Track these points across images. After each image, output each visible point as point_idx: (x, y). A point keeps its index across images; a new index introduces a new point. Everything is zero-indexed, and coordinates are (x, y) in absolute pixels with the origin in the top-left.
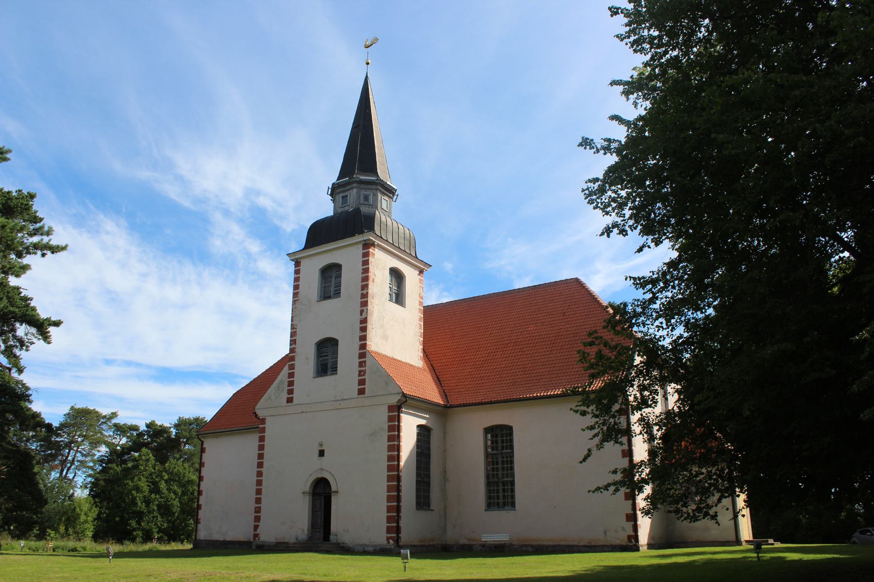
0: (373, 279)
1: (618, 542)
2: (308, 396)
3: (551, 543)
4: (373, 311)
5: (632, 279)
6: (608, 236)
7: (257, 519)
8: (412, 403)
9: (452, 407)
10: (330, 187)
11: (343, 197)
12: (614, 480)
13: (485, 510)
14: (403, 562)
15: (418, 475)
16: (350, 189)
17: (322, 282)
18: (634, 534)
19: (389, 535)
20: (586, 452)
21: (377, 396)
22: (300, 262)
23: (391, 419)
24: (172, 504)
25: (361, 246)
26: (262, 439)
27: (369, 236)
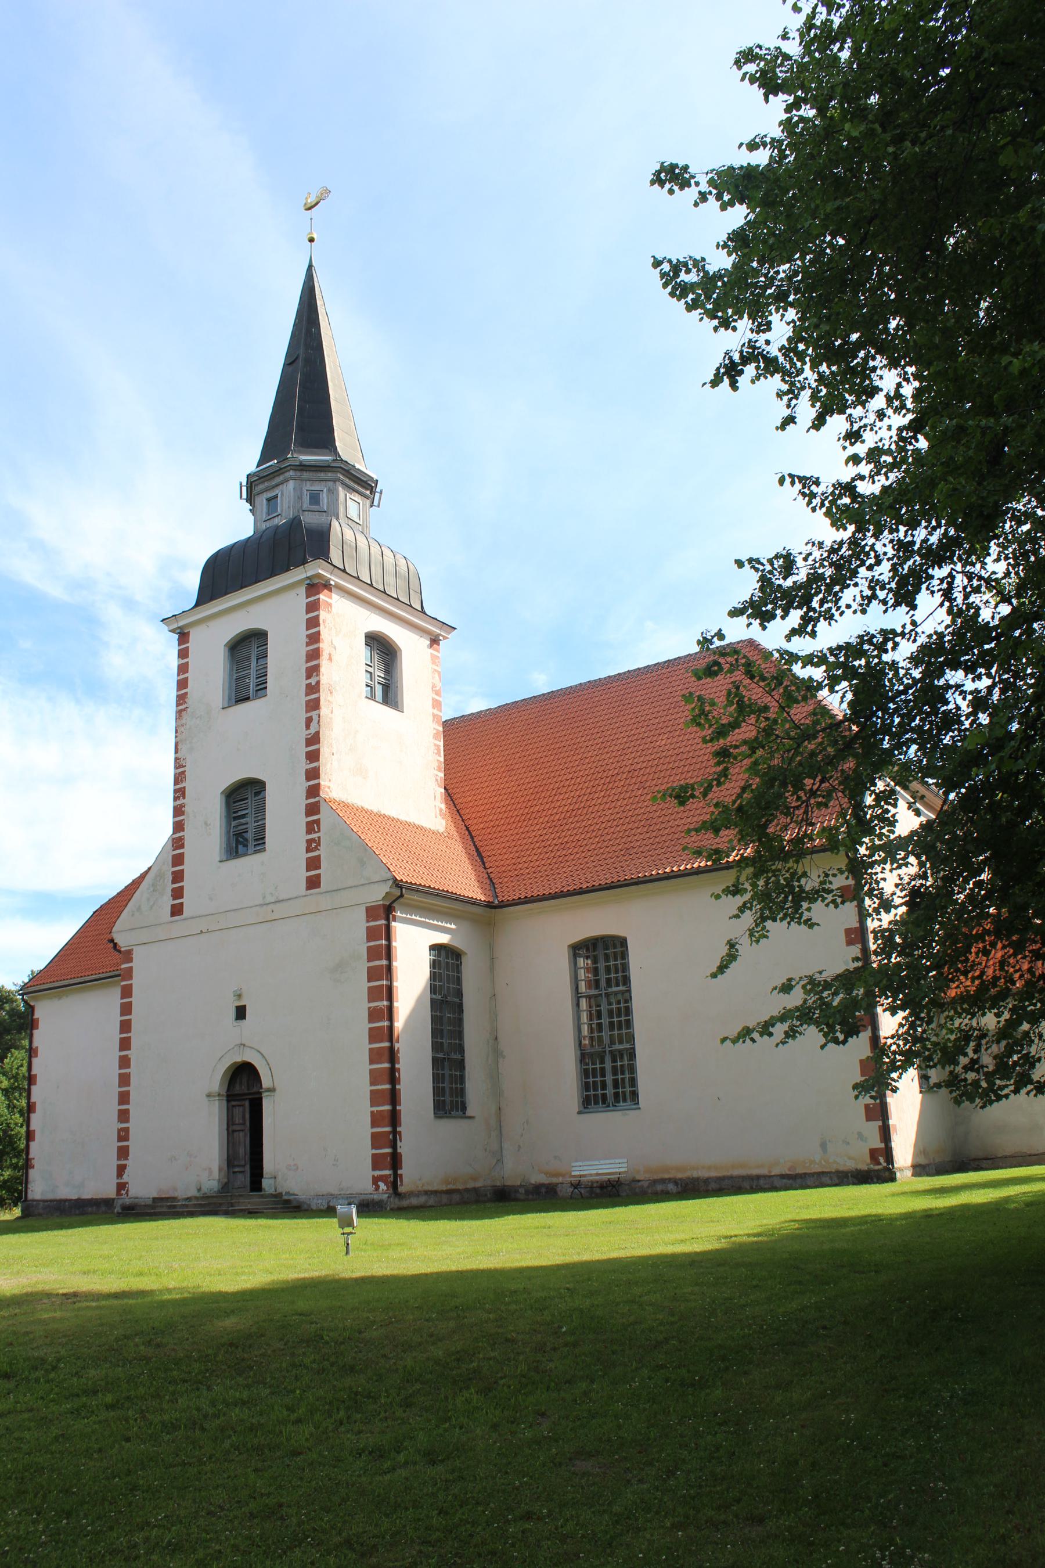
0: (330, 654)
1: (849, 1165)
2: (211, 899)
3: (713, 1174)
4: (331, 719)
5: (796, 480)
6: (734, 386)
7: (123, 1153)
8: (417, 901)
9: (502, 905)
10: (244, 483)
11: (269, 500)
12: (784, 1008)
13: (579, 1113)
14: (344, 1234)
15: (436, 1047)
16: (282, 483)
17: (231, 670)
18: (883, 1145)
19: (377, 1173)
20: (724, 950)
21: (344, 889)
22: (189, 633)
23: (372, 934)
24: (16, 1135)
25: (302, 590)
26: (127, 992)
27: (316, 568)
